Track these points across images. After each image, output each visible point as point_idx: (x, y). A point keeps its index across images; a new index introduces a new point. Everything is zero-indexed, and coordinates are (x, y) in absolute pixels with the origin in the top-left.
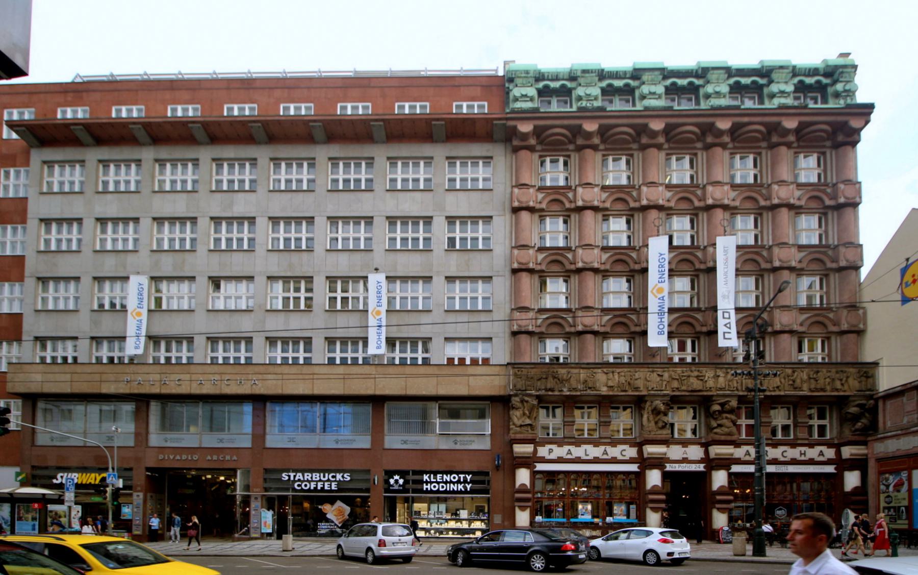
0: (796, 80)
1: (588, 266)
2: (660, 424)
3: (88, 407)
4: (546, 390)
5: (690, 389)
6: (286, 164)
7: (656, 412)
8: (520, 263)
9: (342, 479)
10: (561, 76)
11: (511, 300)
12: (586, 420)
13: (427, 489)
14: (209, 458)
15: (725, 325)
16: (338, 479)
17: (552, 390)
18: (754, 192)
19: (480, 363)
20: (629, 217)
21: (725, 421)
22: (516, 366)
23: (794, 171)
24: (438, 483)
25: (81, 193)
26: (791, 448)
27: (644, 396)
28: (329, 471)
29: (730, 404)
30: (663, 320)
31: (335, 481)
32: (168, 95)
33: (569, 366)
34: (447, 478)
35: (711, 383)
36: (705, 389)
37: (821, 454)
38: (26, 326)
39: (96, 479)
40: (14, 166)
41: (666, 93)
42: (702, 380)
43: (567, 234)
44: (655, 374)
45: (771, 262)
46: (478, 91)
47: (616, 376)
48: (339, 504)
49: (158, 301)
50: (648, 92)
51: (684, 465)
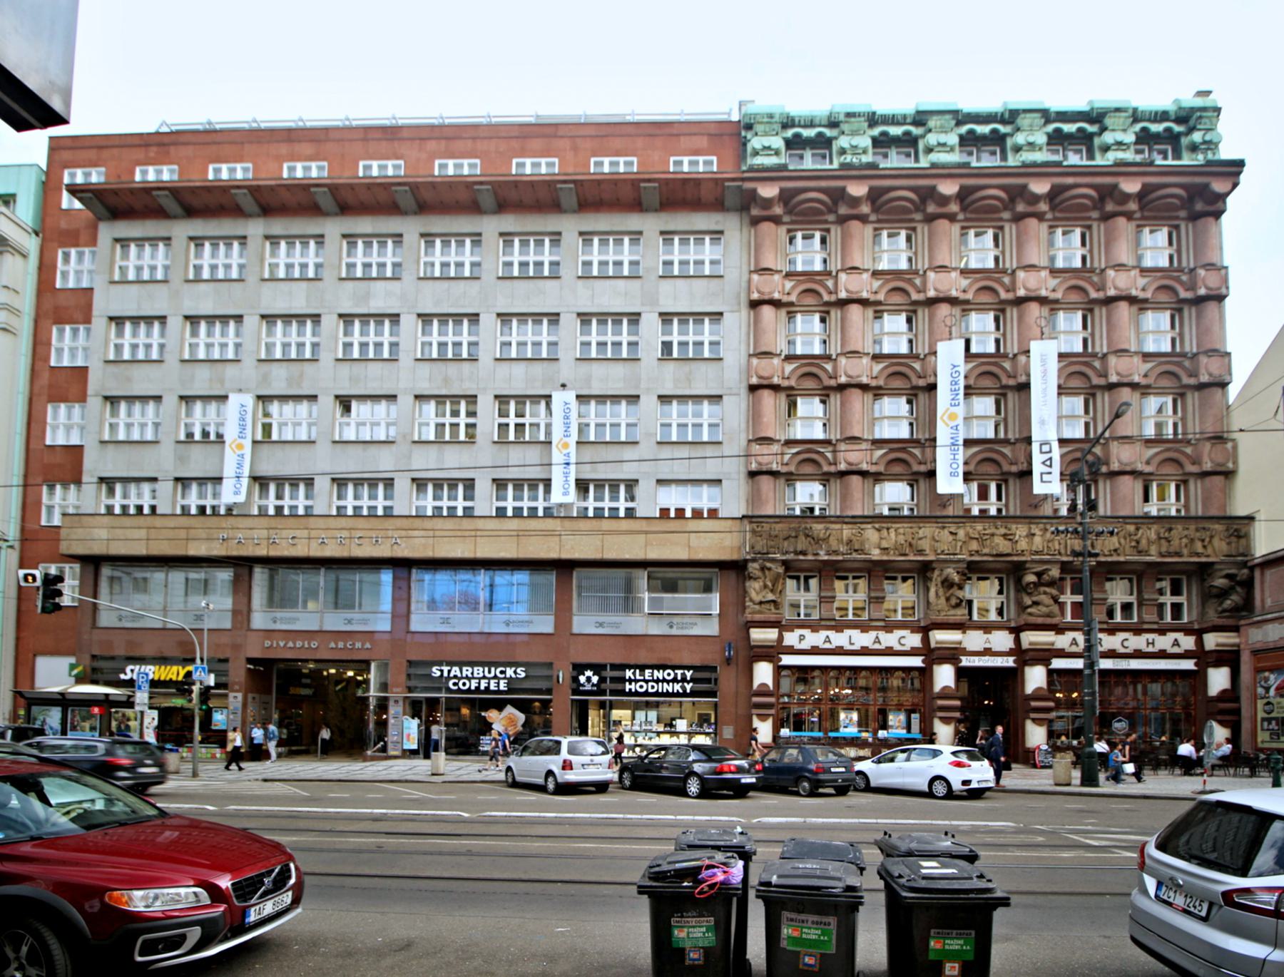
0: (1138, 127)
1: (853, 381)
2: (954, 601)
3: (170, 575)
4: (796, 553)
7: (948, 584)
9: (513, 676)
10: (817, 122)
11: (748, 427)
12: (850, 595)
13: (630, 690)
14: (333, 645)
16: (508, 676)
17: (804, 553)
19: (705, 515)
22: (754, 520)
24: (647, 682)
25: (240, 280)
26: (1135, 634)
27: (931, 562)
28: (496, 665)
29: (1050, 573)
31: (505, 678)
32: (284, 149)
34: (658, 674)
35: (1023, 545)
37: (1176, 643)
39: (178, 674)
40: (76, 245)
42: (1010, 540)
44: (946, 531)
45: (1106, 376)
46: (703, 142)
48: (510, 710)
49: (267, 428)
50: (935, 143)
51: (987, 658)
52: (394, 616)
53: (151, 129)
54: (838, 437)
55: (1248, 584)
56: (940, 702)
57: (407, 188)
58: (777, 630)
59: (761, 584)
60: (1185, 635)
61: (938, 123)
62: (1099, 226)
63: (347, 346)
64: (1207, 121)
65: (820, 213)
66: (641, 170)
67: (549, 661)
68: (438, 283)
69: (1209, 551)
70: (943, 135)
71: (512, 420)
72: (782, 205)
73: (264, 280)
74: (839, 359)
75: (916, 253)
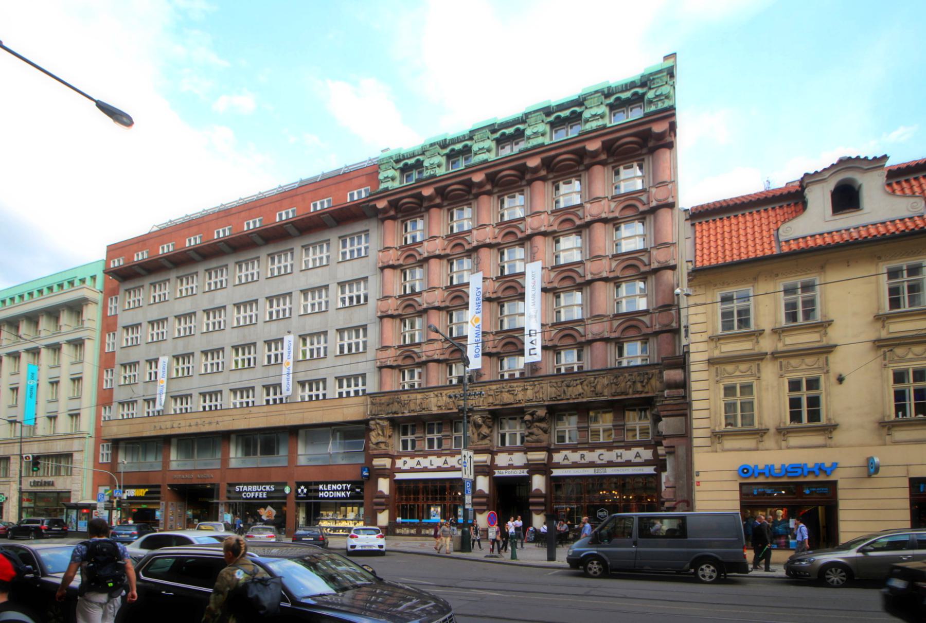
2: (481, 436)
5: (502, 403)
6: (365, 235)
8: (382, 312)
18: (567, 214)
22: (372, 396)
24: (329, 491)
28: (262, 484)
29: (537, 413)
31: (265, 491)
34: (334, 487)
35: (520, 396)
37: (638, 455)
42: (513, 394)
48: (269, 508)
51: (510, 470)
57: (328, 214)
65: (636, 150)
66: (334, 205)
68: (128, 311)
70: (482, 143)
71: (273, 352)
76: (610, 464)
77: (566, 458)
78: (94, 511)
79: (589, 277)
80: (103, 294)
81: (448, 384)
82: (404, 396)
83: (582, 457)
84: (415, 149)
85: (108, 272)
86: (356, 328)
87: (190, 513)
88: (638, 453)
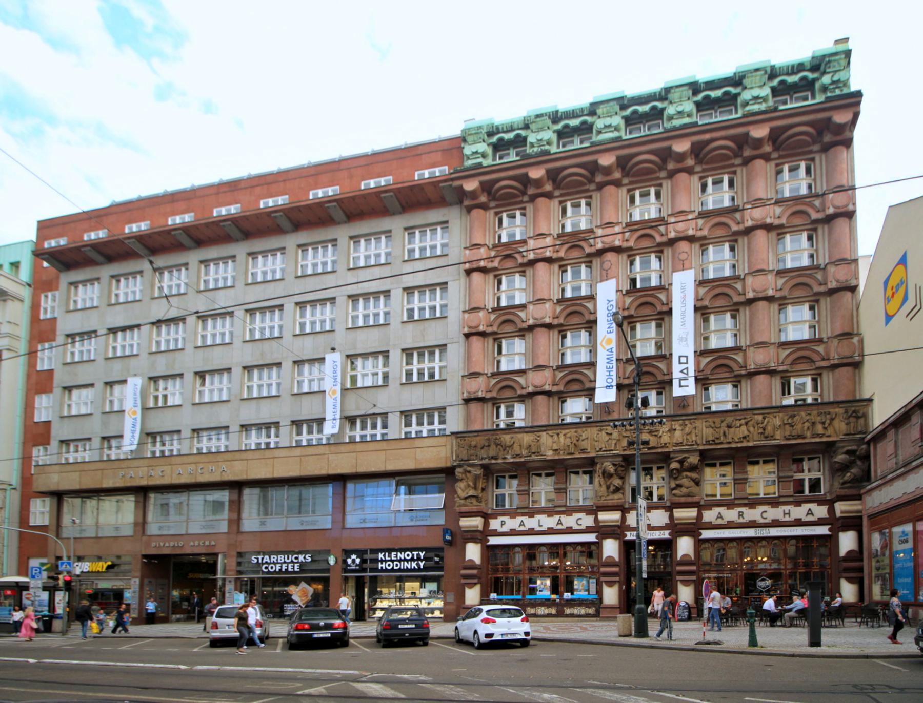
1: (539, 322)
2: (612, 488)
3: (191, 498)
7: (607, 475)
8: (470, 327)
10: (516, 126)
12: (543, 488)
14: (192, 544)
15: (682, 371)
20: (810, 232)
21: (685, 481)
22: (459, 435)
23: (776, 187)
24: (392, 561)
25: (333, 272)
26: (773, 507)
27: (594, 457)
28: (293, 553)
29: (689, 460)
30: (611, 373)
33: (513, 431)
34: (401, 556)
35: (665, 439)
36: (660, 445)
37: (810, 512)
38: (54, 432)
40: (51, 290)
41: (698, 110)
42: (656, 435)
43: (812, 252)
44: (603, 433)
46: (438, 157)
47: (562, 438)
48: (303, 585)
49: (354, 379)
50: (603, 126)
52: (230, 521)
53: (106, 204)
54: (829, 335)
55: (866, 457)
56: (679, 568)
58: (696, 509)
59: (465, 483)
60: (587, 515)
61: (605, 109)
62: (742, 171)
63: (252, 331)
64: (835, 64)
65: (515, 196)
67: (327, 549)
69: (829, 432)
70: (609, 119)
72: (620, 170)
73: (405, 261)
74: (828, 267)
75: (815, 180)
76: (776, 524)
77: (720, 516)
78: (24, 593)
79: (751, 295)
80: (31, 289)
81: (495, 427)
82: (504, 436)
83: (741, 514)
84: (514, 120)
85: (39, 254)
86: (408, 352)
87: (176, 593)
88: (810, 510)
